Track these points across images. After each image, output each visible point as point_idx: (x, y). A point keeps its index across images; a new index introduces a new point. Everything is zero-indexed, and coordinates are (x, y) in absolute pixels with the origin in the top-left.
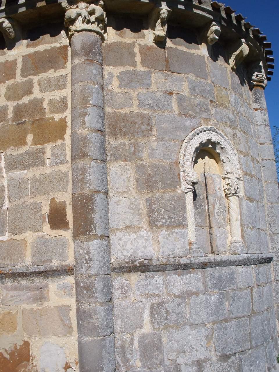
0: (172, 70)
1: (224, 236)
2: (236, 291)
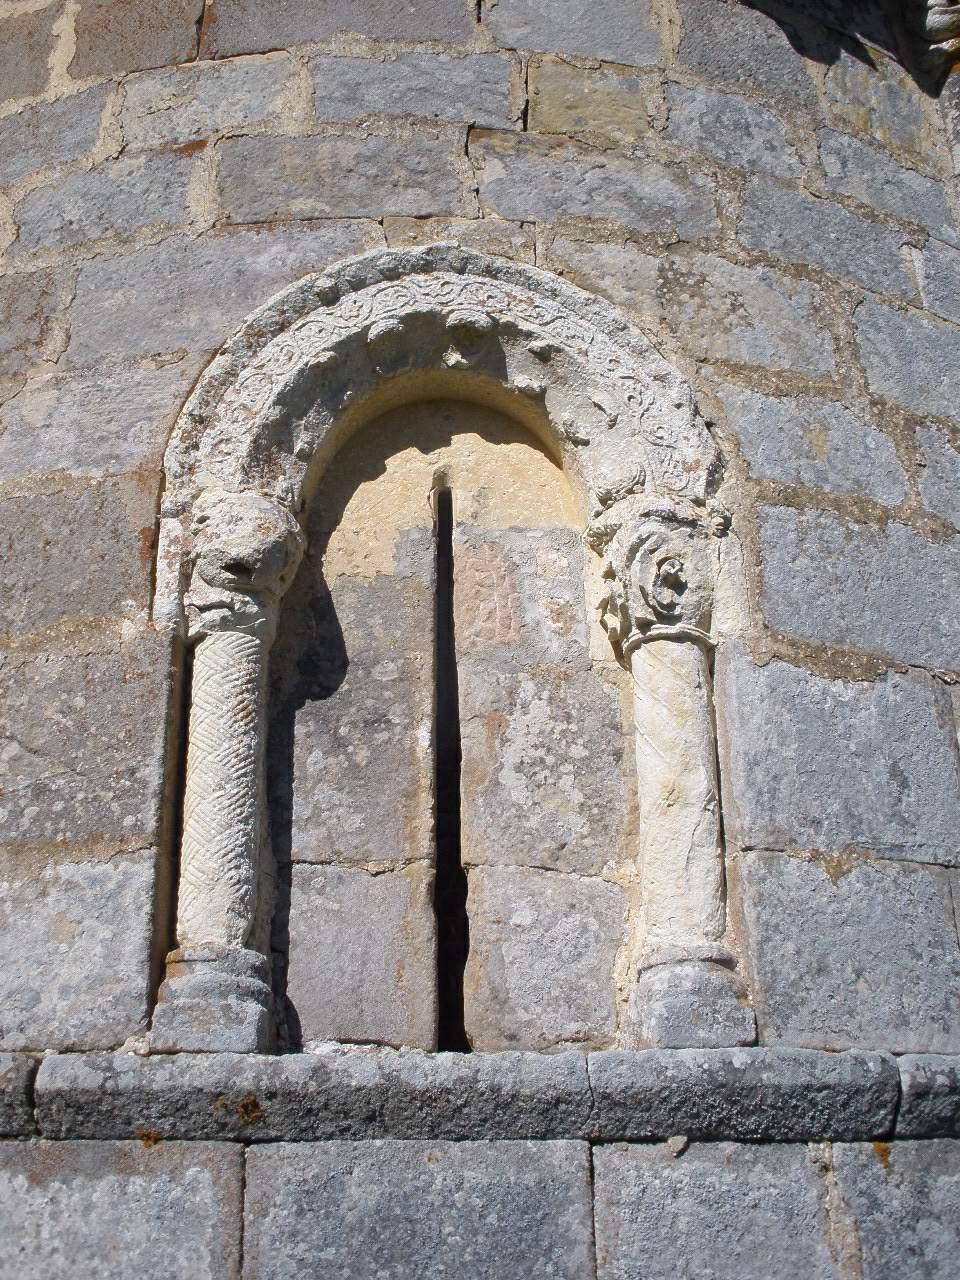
0: (228, 46)
1: (585, 929)
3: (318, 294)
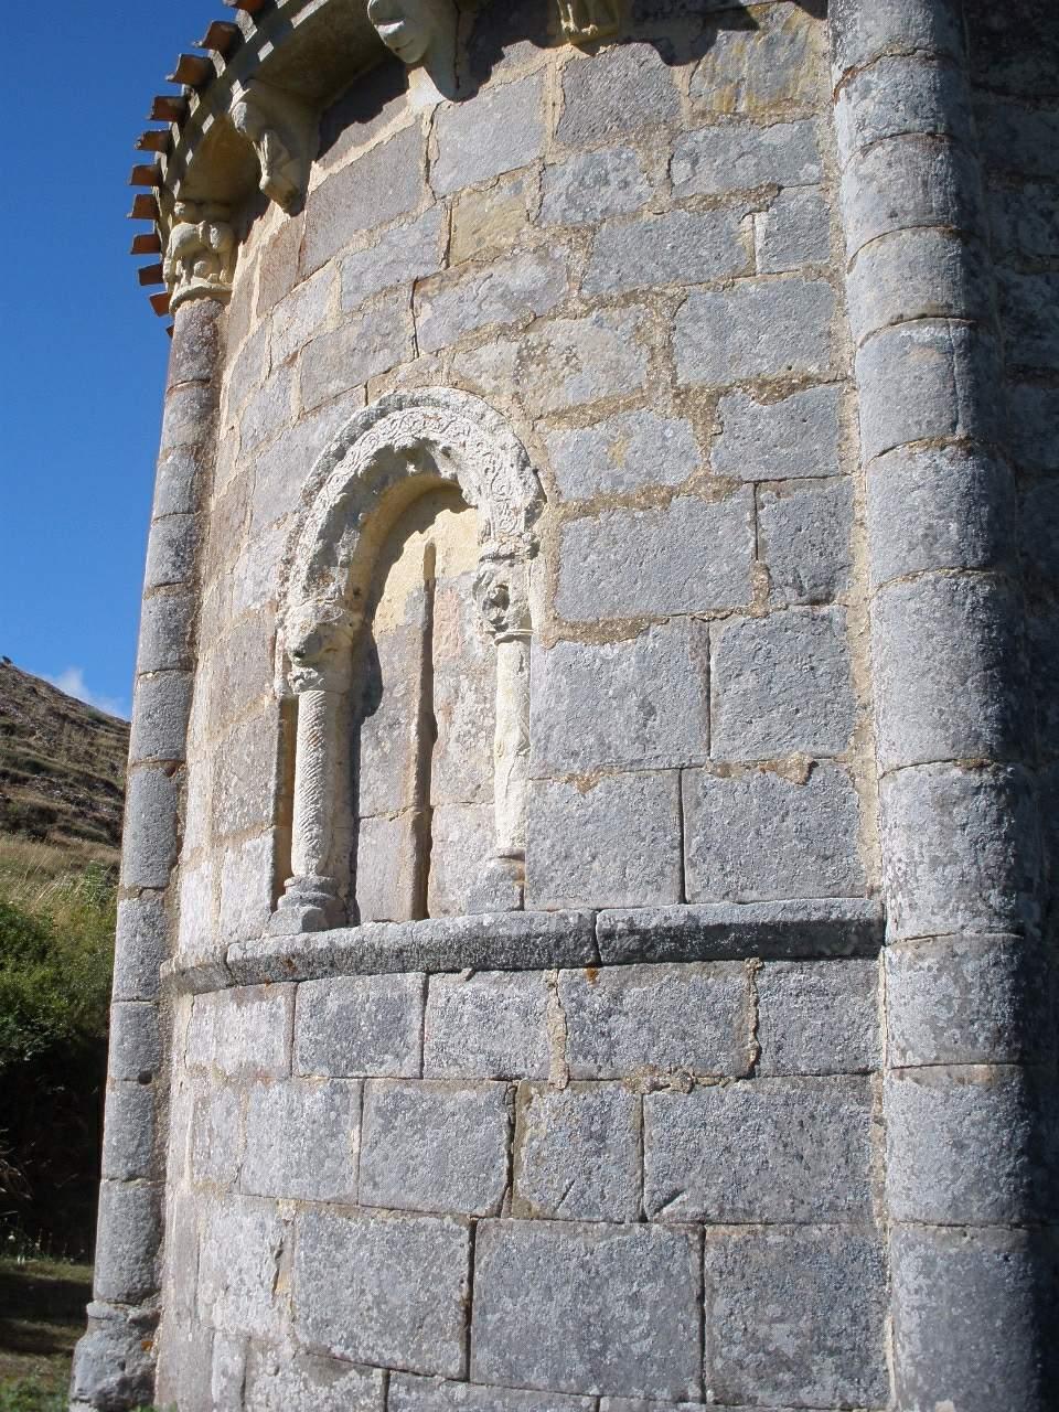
2: (408, 1086)
3: (334, 455)
